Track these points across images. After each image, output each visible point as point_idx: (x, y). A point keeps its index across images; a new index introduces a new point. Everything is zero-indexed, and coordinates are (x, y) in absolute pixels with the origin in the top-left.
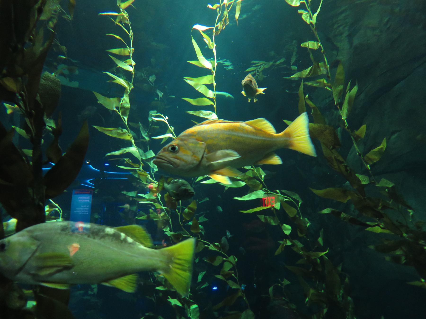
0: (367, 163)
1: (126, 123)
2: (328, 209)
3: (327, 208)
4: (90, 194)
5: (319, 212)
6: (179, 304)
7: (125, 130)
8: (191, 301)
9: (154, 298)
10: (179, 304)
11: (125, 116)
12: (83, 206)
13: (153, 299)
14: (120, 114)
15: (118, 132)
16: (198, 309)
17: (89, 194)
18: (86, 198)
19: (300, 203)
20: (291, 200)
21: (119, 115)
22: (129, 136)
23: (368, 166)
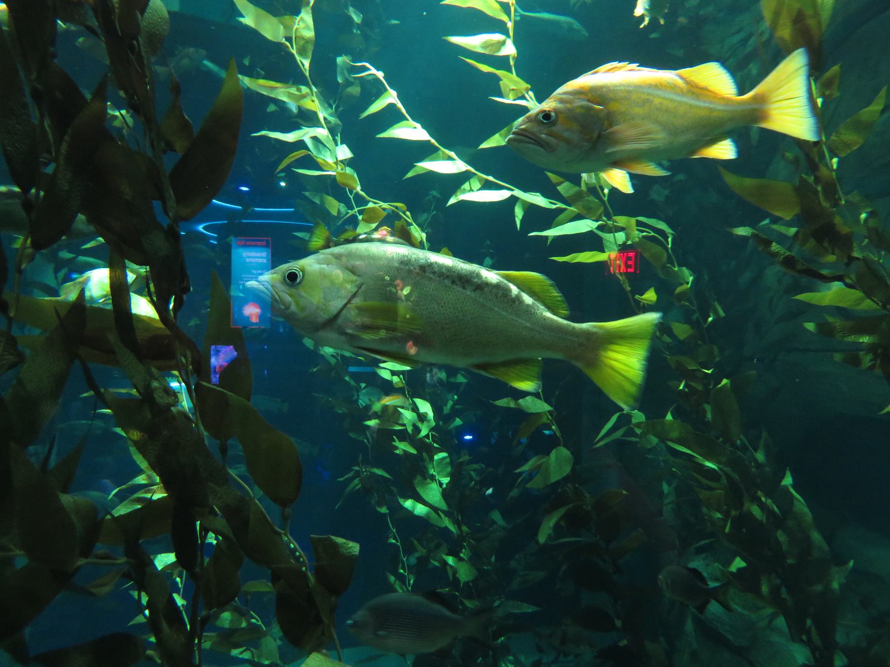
0: (833, 154)
1: (307, 74)
2: (747, 228)
3: (745, 226)
4: (267, 246)
5: (728, 229)
6: (413, 451)
7: (304, 89)
8: (435, 445)
9: (367, 439)
10: (413, 451)
11: (305, 57)
12: (255, 272)
13: (366, 441)
14: (294, 52)
15: (289, 93)
16: (448, 460)
17: (264, 246)
18: (259, 255)
19: (670, 239)
20: (653, 234)
21: (293, 55)
22: (313, 104)
23: (835, 160)
